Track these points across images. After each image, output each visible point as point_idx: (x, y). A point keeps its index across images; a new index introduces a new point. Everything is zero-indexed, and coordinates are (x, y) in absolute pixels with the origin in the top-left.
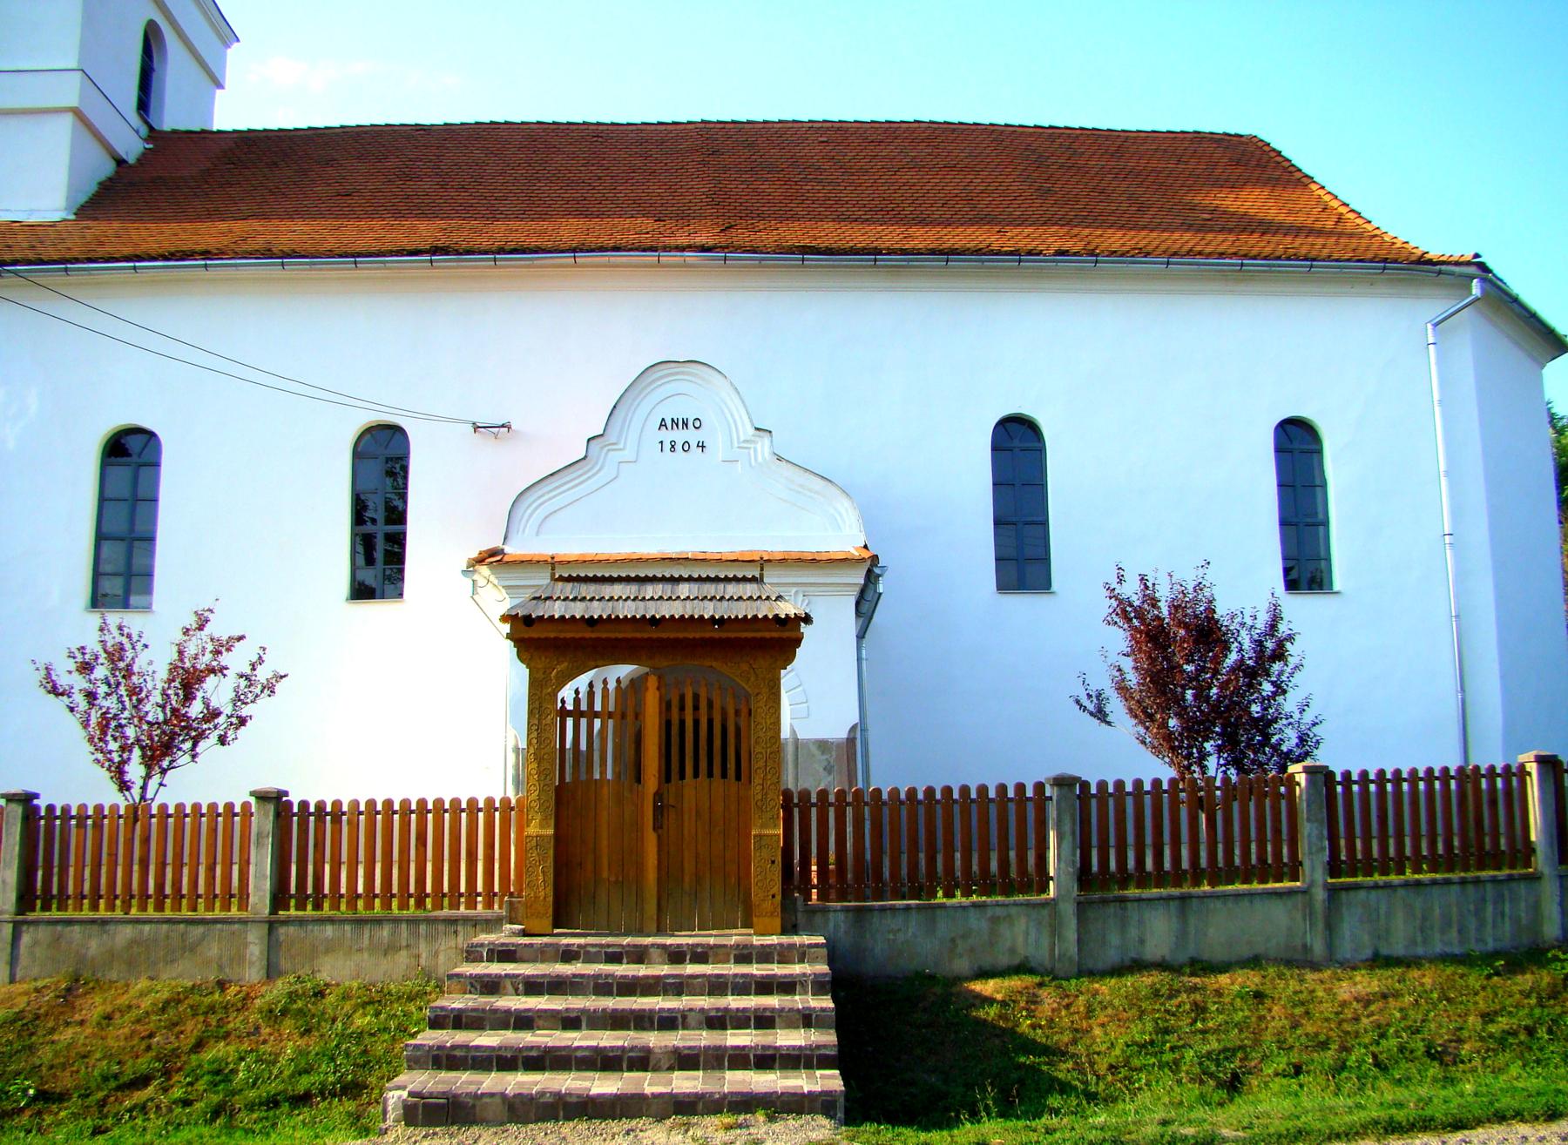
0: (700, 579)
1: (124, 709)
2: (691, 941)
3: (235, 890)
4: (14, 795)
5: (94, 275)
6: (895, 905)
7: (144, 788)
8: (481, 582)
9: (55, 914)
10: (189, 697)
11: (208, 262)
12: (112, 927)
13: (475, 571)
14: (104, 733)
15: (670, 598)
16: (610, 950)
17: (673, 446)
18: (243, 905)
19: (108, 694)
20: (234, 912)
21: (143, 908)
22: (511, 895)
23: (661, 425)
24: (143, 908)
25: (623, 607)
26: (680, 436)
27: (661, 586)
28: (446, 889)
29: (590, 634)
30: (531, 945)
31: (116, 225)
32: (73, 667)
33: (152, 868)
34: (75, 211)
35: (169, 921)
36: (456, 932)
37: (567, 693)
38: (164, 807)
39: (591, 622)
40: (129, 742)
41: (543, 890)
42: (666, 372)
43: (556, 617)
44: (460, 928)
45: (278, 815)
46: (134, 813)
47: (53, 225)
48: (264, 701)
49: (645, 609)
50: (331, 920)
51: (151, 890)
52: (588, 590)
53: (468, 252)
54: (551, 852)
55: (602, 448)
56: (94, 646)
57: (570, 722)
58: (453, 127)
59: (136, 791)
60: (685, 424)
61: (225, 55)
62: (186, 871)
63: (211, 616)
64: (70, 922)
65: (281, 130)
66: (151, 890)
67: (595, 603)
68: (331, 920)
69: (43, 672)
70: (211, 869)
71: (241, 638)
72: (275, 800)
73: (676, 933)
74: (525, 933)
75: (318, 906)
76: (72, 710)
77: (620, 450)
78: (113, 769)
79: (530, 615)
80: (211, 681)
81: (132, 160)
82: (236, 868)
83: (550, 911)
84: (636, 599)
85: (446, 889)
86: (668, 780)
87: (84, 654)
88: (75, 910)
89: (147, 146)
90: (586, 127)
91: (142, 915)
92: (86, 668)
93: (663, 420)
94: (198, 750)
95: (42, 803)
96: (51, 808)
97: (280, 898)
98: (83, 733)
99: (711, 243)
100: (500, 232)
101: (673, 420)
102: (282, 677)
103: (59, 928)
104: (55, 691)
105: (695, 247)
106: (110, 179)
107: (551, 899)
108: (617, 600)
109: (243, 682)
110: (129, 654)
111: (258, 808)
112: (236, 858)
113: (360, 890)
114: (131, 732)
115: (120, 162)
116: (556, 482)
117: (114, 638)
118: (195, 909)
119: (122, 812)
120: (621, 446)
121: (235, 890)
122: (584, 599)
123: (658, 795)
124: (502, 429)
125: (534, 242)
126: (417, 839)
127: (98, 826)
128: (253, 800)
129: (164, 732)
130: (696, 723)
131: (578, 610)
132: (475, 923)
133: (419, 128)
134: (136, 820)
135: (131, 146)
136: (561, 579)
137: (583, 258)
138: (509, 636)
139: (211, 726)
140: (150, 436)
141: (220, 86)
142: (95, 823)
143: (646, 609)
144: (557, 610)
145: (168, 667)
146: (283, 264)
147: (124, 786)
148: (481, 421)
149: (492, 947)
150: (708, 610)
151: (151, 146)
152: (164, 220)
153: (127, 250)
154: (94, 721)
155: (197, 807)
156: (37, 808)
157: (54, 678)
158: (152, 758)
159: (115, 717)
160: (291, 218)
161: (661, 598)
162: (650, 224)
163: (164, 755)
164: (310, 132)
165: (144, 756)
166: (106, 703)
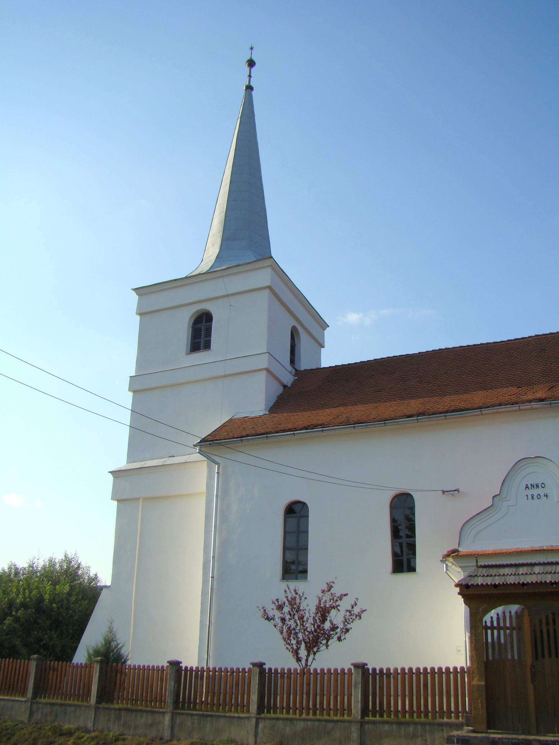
0: (544, 564)
1: (297, 625)
2: (552, 739)
3: (346, 707)
4: (256, 663)
5: (277, 438)
6: (146, 687)
7: (307, 660)
8: (450, 564)
9: (272, 715)
10: (324, 620)
11: (323, 429)
12: (295, 722)
13: (446, 560)
14: (289, 637)
15: (531, 574)
16: (514, 741)
17: (532, 497)
18: (350, 714)
19: (290, 619)
20: (346, 717)
21: (308, 714)
22: (467, 713)
23: (526, 487)
24: (308, 714)
25: (509, 579)
26: (535, 492)
27: (526, 568)
28: (437, 710)
29: (495, 591)
30: (476, 737)
31: (285, 415)
32: (275, 607)
33: (311, 696)
34: (268, 409)
35: (319, 720)
36: (443, 730)
37: (487, 618)
38: (315, 670)
39: (495, 586)
40: (299, 640)
41: (482, 712)
42: (525, 463)
43: (479, 584)
44: (444, 728)
45: (363, 674)
46: (303, 672)
47: (260, 417)
48: (357, 622)
49: (519, 579)
50: (387, 722)
51: (311, 706)
52: (493, 571)
53: (433, 414)
54: (484, 693)
55: (500, 500)
56: (282, 599)
57: (489, 631)
58: (422, 354)
59: (303, 662)
60: (537, 486)
61: (324, 333)
62: (325, 698)
63: (333, 585)
64: (278, 719)
65: (349, 364)
66: (311, 706)
67: (497, 577)
68: (387, 722)
69: (262, 610)
70: (336, 698)
71: (346, 595)
72: (361, 667)
73: (548, 735)
74: (474, 731)
75: (381, 716)
76: (275, 626)
77: (508, 500)
78: (294, 652)
79: (468, 584)
80: (333, 612)
81: (289, 385)
82: (346, 697)
83: (485, 721)
84: (515, 574)
85: (437, 710)
86: (537, 658)
87: (278, 602)
88: (280, 713)
89: (295, 378)
90: (482, 346)
91: (308, 717)
92: (280, 608)
93: (527, 485)
94: (329, 643)
95: (266, 667)
96: (270, 669)
97: (365, 711)
98: (281, 636)
99: (544, 396)
100: (448, 401)
101: (531, 485)
102: (364, 611)
103: (274, 721)
104: (268, 619)
105: (537, 399)
106: (281, 394)
107: (485, 715)
108: (507, 575)
109: (348, 614)
110: (298, 601)
111: (355, 671)
112: (346, 692)
113: (400, 708)
114: (300, 636)
115: (285, 387)
116: (479, 517)
117: (293, 595)
118: (329, 716)
119: (299, 671)
120: (508, 498)
121: (346, 707)
122: (491, 575)
123: (533, 666)
124: (456, 492)
125: (462, 405)
126: (424, 686)
127: (289, 678)
128: (352, 667)
129: (314, 636)
130: (548, 631)
131: (489, 581)
132: (451, 726)
133: (408, 356)
134: (304, 674)
135: (288, 379)
136: (481, 567)
137: (485, 411)
138: (459, 594)
139: (334, 633)
140: (304, 504)
141: (323, 347)
142: (287, 676)
143: (493, 580)
144: (480, 581)
145: (315, 607)
146: (354, 427)
147: (299, 660)
148: (445, 489)
149: (458, 737)
150: (549, 579)
151: (297, 378)
152: (304, 410)
153: (290, 426)
154: (285, 631)
155: (238, 669)
156: (265, 669)
157: (267, 612)
158: (310, 647)
159: (294, 629)
160: (356, 405)
161: (526, 574)
162: (515, 390)
163: (314, 646)
164: (361, 364)
165: (306, 646)
166: (289, 623)
